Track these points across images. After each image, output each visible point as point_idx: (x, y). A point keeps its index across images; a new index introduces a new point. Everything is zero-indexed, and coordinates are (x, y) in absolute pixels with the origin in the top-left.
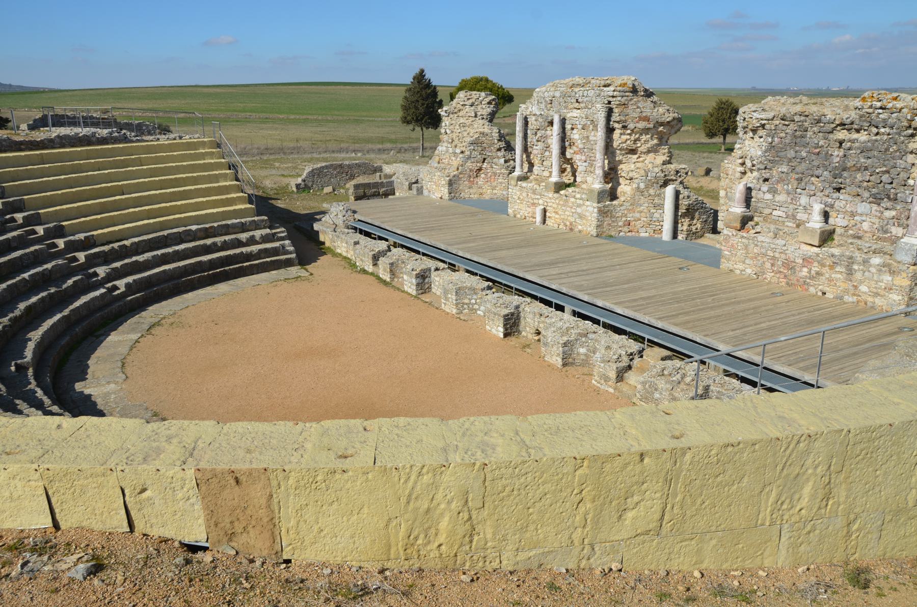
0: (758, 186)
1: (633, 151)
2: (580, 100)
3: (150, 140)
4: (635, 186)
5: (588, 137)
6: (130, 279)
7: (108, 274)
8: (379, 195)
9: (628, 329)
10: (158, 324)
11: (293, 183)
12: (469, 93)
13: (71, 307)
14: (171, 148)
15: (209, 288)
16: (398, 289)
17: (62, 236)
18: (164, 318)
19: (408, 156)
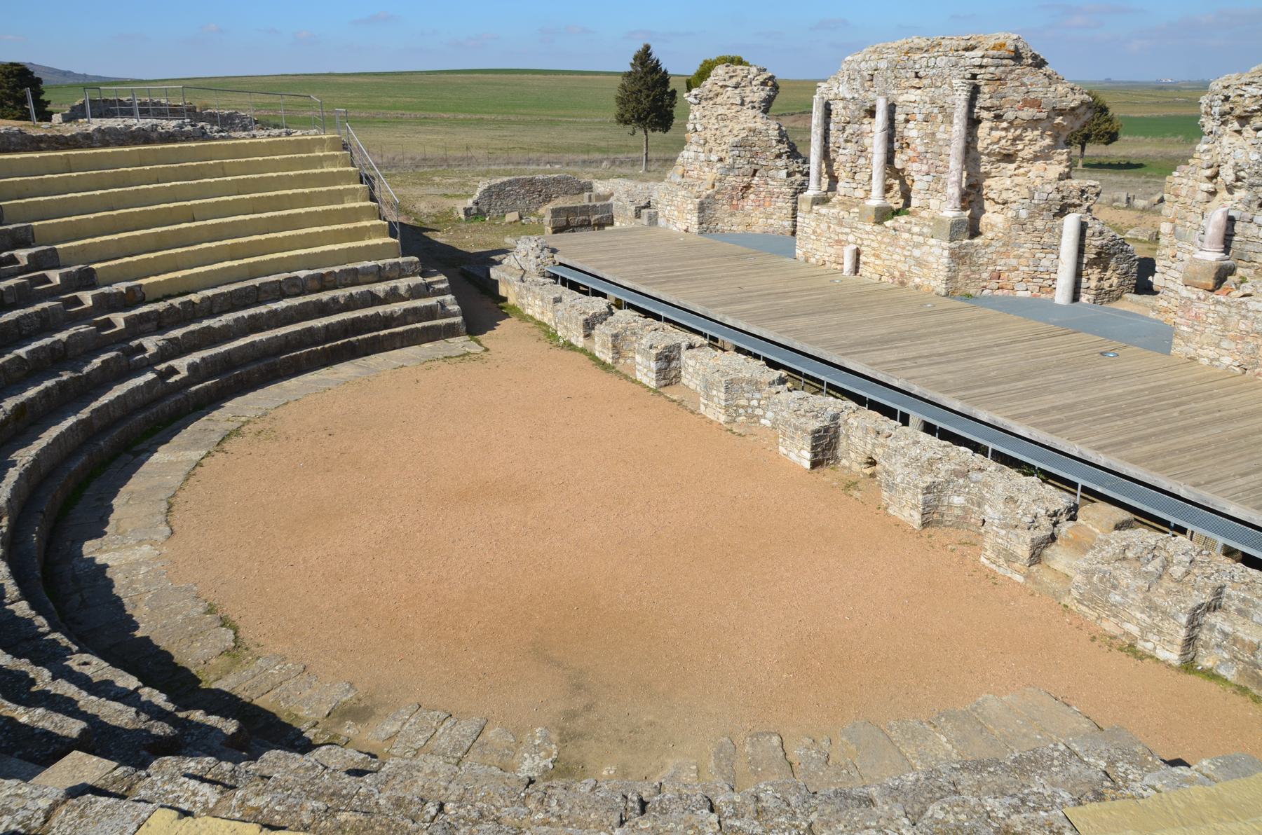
0: (1249, 215)
1: (1008, 158)
2: (921, 74)
3: (241, 138)
4: (1011, 214)
5: (934, 134)
6: (196, 357)
7: (161, 349)
8: (589, 224)
9: (1038, 464)
10: (237, 432)
11: (460, 206)
12: (731, 68)
13: (95, 405)
14: (271, 148)
15: (324, 371)
16: (626, 377)
17: (92, 286)
18: (248, 422)
19: (625, 170)
